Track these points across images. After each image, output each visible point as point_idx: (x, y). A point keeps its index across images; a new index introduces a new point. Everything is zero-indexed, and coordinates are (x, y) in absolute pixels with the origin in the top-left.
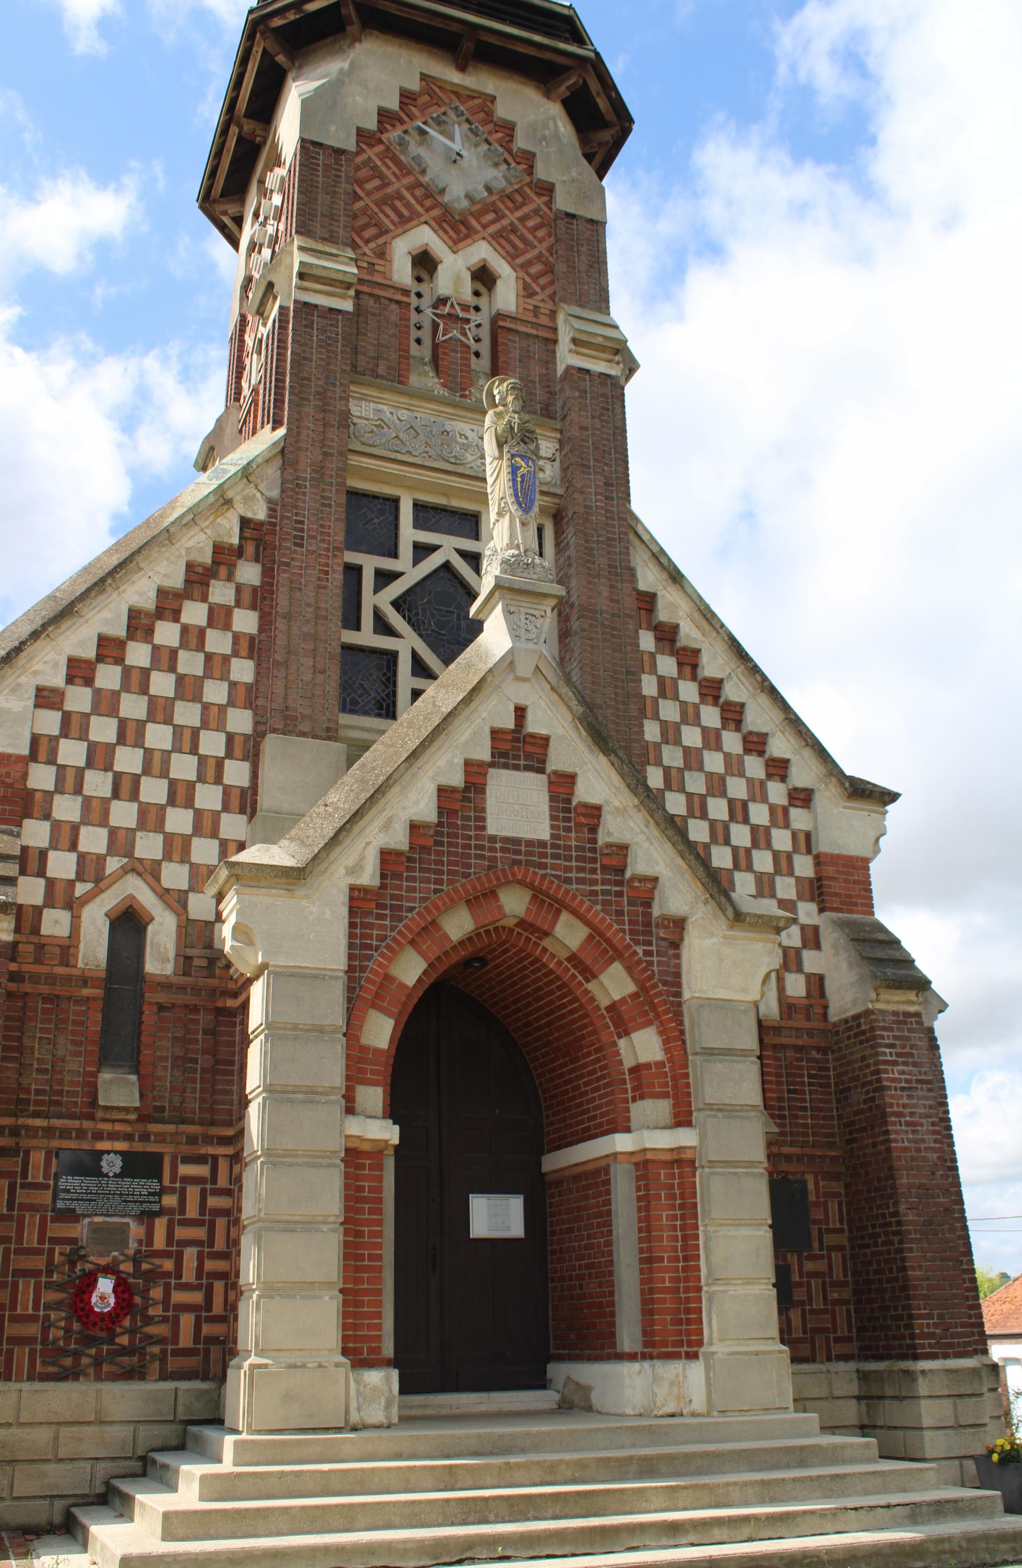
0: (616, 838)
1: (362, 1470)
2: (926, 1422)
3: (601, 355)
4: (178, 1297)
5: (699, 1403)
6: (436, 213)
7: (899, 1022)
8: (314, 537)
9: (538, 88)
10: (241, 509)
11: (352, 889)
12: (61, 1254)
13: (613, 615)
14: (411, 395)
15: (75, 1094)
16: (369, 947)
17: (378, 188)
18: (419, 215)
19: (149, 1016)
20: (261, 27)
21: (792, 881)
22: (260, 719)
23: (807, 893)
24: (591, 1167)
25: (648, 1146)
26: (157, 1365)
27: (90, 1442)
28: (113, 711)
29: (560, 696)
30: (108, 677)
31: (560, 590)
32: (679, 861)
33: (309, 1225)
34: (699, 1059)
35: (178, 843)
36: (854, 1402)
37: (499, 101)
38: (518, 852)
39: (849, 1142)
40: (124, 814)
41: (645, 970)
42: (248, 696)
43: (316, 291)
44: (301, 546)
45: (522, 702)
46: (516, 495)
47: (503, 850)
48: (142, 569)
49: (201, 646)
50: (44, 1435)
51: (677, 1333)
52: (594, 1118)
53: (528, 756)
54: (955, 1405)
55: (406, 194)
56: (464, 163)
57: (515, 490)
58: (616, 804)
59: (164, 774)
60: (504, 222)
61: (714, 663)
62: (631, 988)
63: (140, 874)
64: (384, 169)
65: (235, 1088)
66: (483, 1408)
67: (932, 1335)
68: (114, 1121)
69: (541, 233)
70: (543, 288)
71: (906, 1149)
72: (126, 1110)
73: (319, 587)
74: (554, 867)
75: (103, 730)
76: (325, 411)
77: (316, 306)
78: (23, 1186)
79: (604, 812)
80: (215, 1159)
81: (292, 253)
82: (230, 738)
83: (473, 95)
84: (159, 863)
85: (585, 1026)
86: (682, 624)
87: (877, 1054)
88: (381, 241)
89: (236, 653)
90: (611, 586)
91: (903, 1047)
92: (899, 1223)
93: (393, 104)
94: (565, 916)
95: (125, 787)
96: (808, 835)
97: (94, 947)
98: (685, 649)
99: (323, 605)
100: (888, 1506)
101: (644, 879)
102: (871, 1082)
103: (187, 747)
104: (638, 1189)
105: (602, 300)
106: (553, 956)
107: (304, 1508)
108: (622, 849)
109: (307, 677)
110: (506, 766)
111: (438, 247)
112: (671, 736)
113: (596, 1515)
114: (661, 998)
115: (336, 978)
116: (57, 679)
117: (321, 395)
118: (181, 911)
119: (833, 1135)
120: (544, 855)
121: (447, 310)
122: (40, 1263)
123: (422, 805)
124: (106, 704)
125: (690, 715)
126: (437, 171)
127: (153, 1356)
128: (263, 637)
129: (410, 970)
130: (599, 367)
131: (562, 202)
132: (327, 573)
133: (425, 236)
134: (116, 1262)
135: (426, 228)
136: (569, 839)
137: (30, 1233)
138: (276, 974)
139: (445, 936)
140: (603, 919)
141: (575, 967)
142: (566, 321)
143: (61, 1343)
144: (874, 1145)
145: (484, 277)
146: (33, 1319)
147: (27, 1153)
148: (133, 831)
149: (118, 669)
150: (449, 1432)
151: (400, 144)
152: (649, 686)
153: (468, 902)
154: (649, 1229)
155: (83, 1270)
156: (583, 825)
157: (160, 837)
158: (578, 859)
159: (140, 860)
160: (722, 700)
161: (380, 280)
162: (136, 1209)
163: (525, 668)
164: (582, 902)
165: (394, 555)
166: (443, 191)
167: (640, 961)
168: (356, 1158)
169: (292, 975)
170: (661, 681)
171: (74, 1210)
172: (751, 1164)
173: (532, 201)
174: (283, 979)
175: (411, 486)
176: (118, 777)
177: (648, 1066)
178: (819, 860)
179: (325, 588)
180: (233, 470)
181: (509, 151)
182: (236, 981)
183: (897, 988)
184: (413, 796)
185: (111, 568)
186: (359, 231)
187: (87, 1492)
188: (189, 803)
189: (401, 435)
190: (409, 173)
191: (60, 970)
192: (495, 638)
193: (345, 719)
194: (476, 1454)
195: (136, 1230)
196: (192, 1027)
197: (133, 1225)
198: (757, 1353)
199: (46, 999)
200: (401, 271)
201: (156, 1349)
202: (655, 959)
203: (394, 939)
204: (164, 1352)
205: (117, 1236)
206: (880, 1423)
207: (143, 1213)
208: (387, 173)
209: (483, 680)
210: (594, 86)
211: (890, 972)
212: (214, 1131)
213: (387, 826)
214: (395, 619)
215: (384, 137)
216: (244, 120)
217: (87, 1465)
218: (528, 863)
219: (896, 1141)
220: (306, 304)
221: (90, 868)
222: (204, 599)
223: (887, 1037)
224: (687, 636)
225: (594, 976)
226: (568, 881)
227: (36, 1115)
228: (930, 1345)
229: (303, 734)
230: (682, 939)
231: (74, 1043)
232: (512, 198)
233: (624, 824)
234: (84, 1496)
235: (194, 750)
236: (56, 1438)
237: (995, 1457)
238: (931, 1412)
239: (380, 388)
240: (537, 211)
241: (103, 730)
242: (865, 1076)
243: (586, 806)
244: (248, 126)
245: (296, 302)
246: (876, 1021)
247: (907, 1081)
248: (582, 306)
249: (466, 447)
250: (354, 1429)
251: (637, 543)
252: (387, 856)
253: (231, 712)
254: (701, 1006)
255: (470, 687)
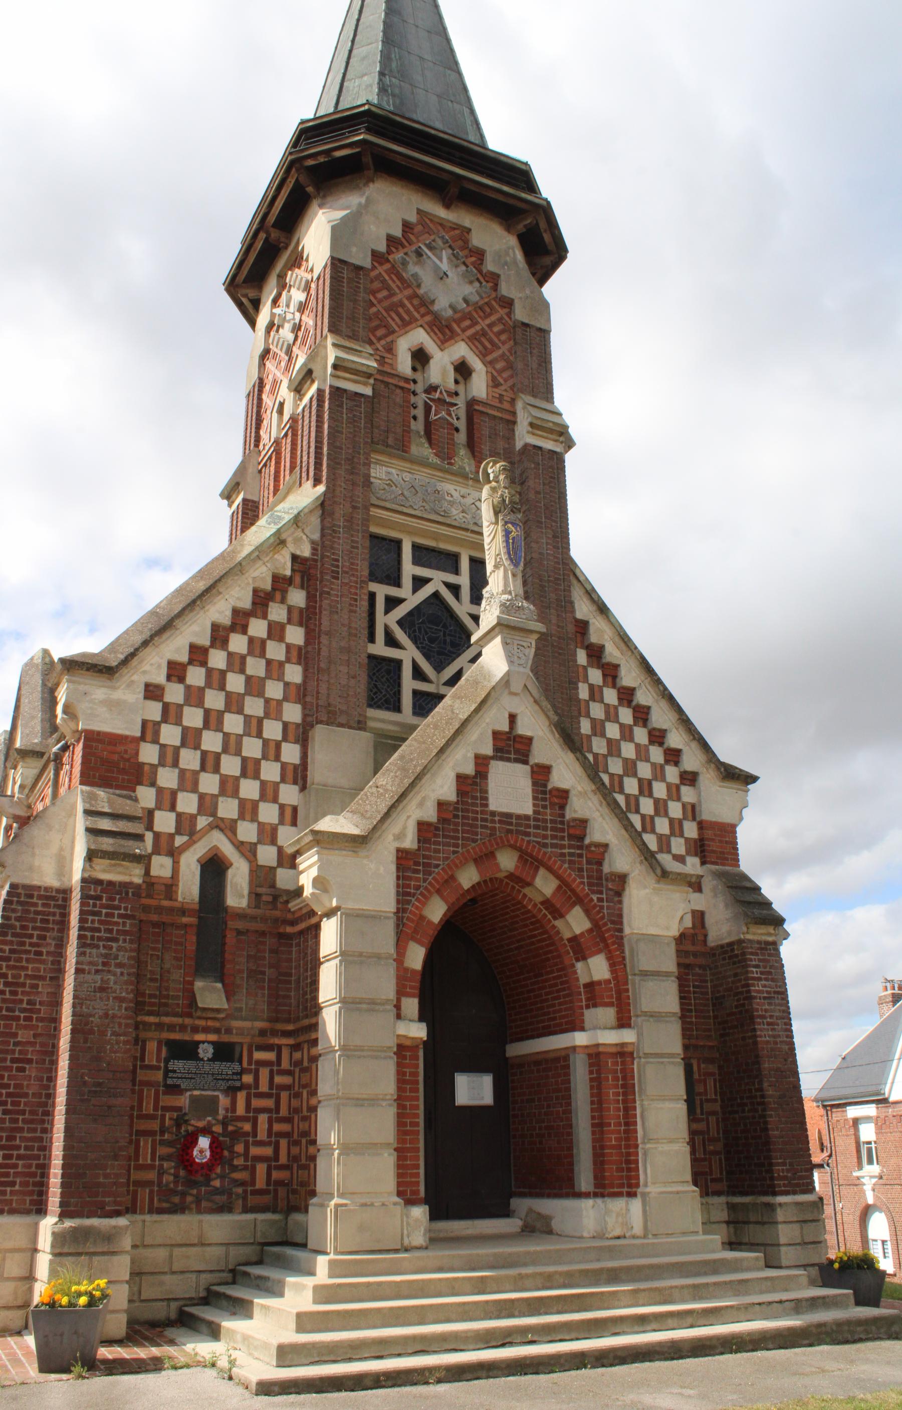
0: (580, 815)
1: (423, 1281)
2: (783, 1240)
3: (550, 436)
4: (255, 1151)
5: (638, 1229)
6: (428, 318)
7: (761, 949)
8: (347, 573)
9: (501, 224)
10: (291, 548)
11: (398, 850)
12: (170, 1119)
13: (559, 638)
14: (412, 462)
15: (177, 997)
16: (409, 894)
17: (386, 298)
18: (416, 320)
19: (230, 938)
20: (297, 165)
21: (682, 841)
22: (307, 712)
23: (693, 849)
24: (552, 1055)
25: (601, 1042)
26: (240, 1202)
27: (195, 1259)
28: (200, 703)
29: (541, 707)
30: (196, 676)
31: (540, 627)
32: (623, 832)
33: (373, 1101)
34: (637, 978)
35: (249, 806)
36: (724, 1225)
37: (473, 232)
38: (511, 824)
39: (722, 1036)
40: (209, 783)
41: (599, 912)
42: (300, 694)
43: (345, 379)
44: (337, 578)
45: (514, 711)
46: (509, 553)
47: (500, 822)
48: (220, 593)
49: (263, 654)
50: (162, 1253)
51: (619, 1177)
52: (554, 1019)
53: (517, 752)
54: (802, 1228)
55: (406, 302)
56: (448, 281)
57: (508, 549)
58: (580, 789)
59: (238, 753)
60: (478, 328)
61: (629, 676)
62: (587, 925)
63: (222, 830)
64: (390, 282)
65: (292, 994)
66: (470, 1232)
67: (785, 1178)
68: (207, 1019)
69: (503, 337)
70: (506, 381)
71: (768, 1042)
72: (218, 1011)
73: (351, 611)
74: (536, 835)
75: (193, 718)
76: (352, 473)
77: (345, 391)
78: (142, 1067)
79: (571, 795)
80: (279, 1048)
81: (326, 347)
82: (286, 725)
83: (456, 227)
84: (235, 821)
85: (551, 952)
86: (607, 645)
87: (747, 972)
88: (389, 339)
89: (288, 660)
90: (558, 616)
91: (765, 967)
92: (763, 1096)
93: (398, 232)
94: (542, 872)
95: (210, 762)
96: (693, 807)
97: (190, 886)
98: (608, 664)
99: (353, 625)
100: (781, 1302)
101: (598, 845)
102: (742, 993)
103: (254, 733)
104: (591, 1072)
105: (547, 392)
106: (530, 900)
107: (391, 1309)
108: (583, 823)
109: (344, 682)
110: (502, 759)
111: (431, 346)
112: (598, 731)
113: (586, 1310)
114: (608, 934)
115: (388, 918)
116: (160, 678)
117: (350, 460)
118: (252, 858)
119: (709, 1030)
120: (529, 826)
121: (437, 395)
122: (155, 1126)
123: (446, 788)
124: (195, 697)
125: (611, 715)
126: (428, 285)
127: (237, 1195)
128: (310, 648)
129: (436, 911)
130: (548, 445)
131: (520, 314)
132: (356, 600)
133: (419, 337)
134: (210, 1125)
135: (421, 330)
136: (546, 814)
137: (148, 1103)
138: (347, 915)
139: (460, 885)
140: (570, 875)
141: (546, 909)
142: (524, 408)
143: (172, 1185)
144: (744, 1039)
145: (463, 370)
146: (152, 1167)
147: (144, 1042)
148: (216, 796)
149: (203, 670)
150: (475, 1252)
151: (403, 264)
152: (583, 692)
153: (475, 861)
154: (600, 1102)
155: (187, 1131)
156: (556, 804)
157: (236, 802)
158: (552, 829)
159: (222, 819)
160: (634, 703)
161: (389, 370)
162: (223, 1085)
163: (516, 686)
164: (555, 862)
165: (398, 584)
166: (433, 302)
167: (595, 906)
168: (403, 1050)
169: (358, 916)
170: (592, 687)
171: (179, 1086)
172: (671, 1055)
173: (497, 312)
174: (354, 920)
175: (410, 531)
176: (204, 754)
177: (599, 983)
178: (701, 825)
179: (355, 612)
180: (287, 518)
181: (480, 271)
182: (294, 913)
183: (762, 924)
184: (439, 781)
185: (200, 592)
186: (374, 330)
187: (193, 1295)
188: (256, 776)
189: (405, 493)
190: (409, 286)
191: (166, 903)
192: (494, 660)
193: (372, 713)
194: (491, 1267)
195: (224, 1101)
196: (262, 947)
197: (221, 1097)
198: (678, 1193)
199: (155, 925)
200: (404, 364)
201: (240, 1190)
202: (605, 904)
203: (426, 888)
204: (245, 1192)
205: (208, 1106)
206: (746, 1240)
207: (229, 1088)
208: (393, 286)
209: (488, 695)
210: (543, 225)
211: (756, 912)
212: (280, 1026)
213: (421, 804)
214: (400, 635)
215: (390, 257)
216: (272, 230)
217: (194, 1276)
218: (518, 832)
219: (761, 1036)
220: (338, 389)
221: (185, 824)
222: (265, 617)
223: (754, 960)
224: (611, 654)
225: (562, 916)
226: (545, 845)
227: (150, 1013)
228: (784, 1185)
229: (341, 725)
230: (623, 889)
231: (177, 959)
232: (484, 309)
233: (584, 804)
234: (191, 1299)
235: (259, 735)
236: (171, 1256)
237: (836, 1265)
238: (785, 1233)
239: (391, 455)
240: (500, 320)
241: (193, 718)
242: (737, 988)
243: (558, 790)
244: (275, 234)
245: (331, 386)
246: (747, 948)
247: (768, 992)
248: (534, 396)
249: (452, 503)
250: (406, 1250)
251: (574, 582)
252: (423, 827)
253: (286, 705)
254: (638, 940)
255: (479, 700)
